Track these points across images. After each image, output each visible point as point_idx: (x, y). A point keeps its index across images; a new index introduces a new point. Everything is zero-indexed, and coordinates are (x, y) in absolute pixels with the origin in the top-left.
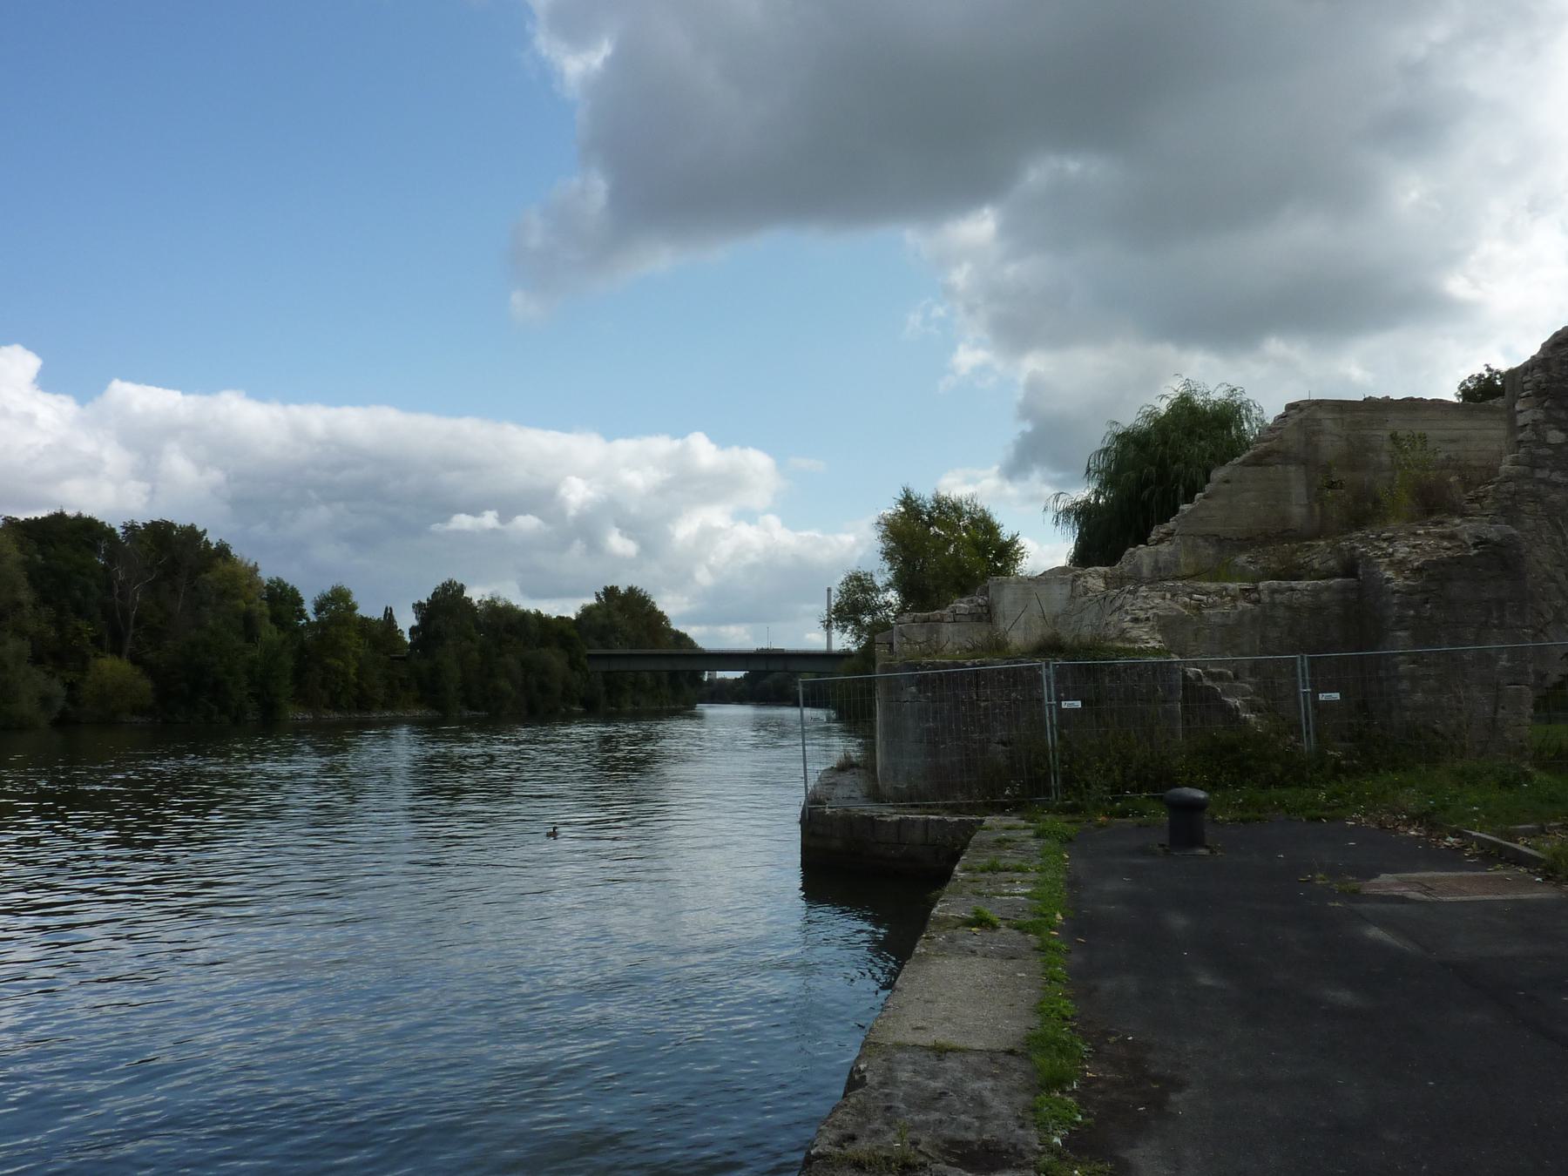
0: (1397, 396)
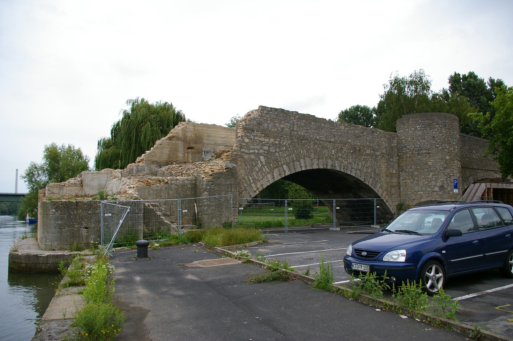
0: (318, 116)
